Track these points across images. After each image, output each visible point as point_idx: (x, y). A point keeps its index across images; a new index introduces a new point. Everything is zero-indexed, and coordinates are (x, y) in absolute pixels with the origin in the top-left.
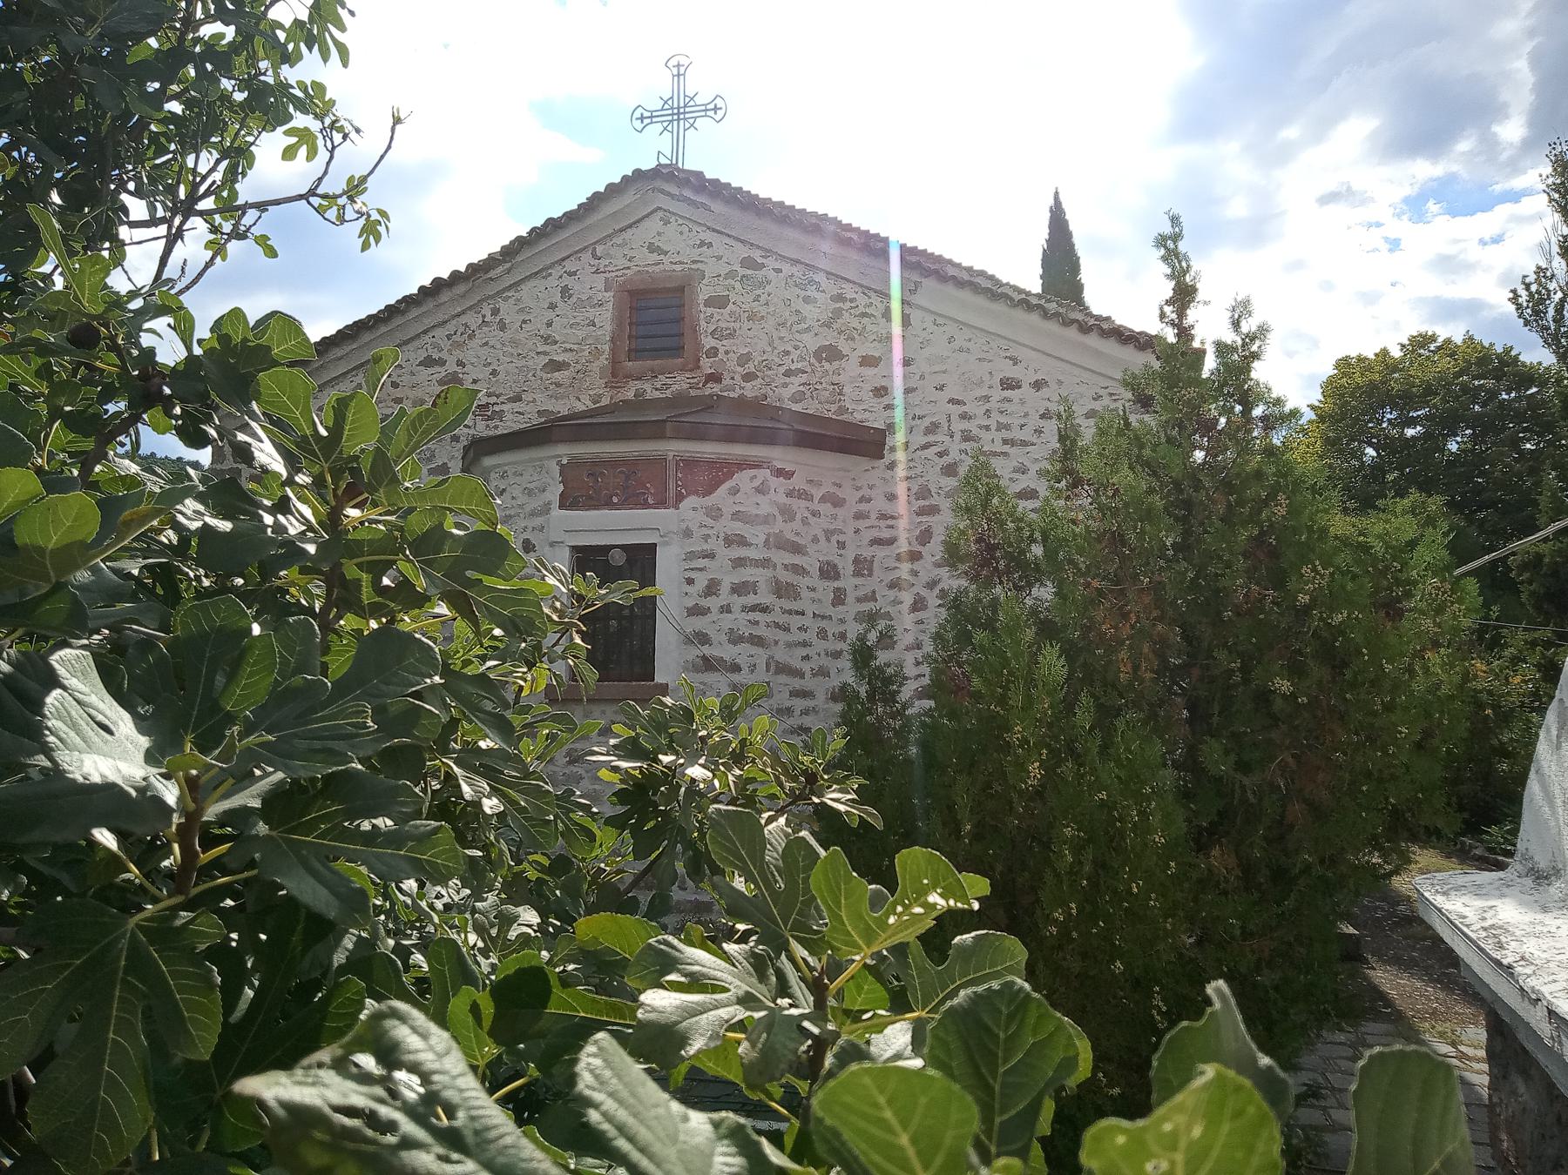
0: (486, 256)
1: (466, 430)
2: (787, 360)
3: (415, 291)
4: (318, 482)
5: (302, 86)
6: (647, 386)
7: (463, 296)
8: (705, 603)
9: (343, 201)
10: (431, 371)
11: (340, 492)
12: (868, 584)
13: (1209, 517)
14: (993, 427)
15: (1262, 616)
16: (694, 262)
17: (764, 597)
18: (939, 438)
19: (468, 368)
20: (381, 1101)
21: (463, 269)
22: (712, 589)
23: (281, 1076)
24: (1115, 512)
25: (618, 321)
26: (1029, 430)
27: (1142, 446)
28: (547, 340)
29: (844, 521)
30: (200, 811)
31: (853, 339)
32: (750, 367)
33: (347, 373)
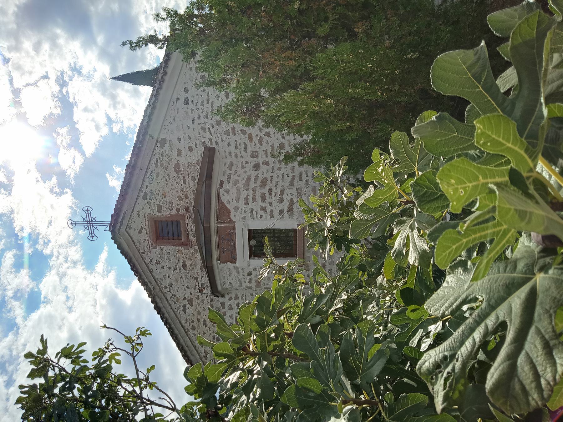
0: (145, 291)
1: (209, 296)
2: (180, 183)
3: (159, 315)
4: (242, 360)
5: (94, 359)
6: (191, 233)
7: (160, 299)
8: (269, 212)
9: (134, 344)
10: (187, 309)
11: (245, 353)
12: (261, 153)
13: (236, 31)
14: (202, 107)
15: (272, 12)
16: (145, 217)
17: (266, 191)
18: (207, 127)
19: (186, 296)
20: (442, 375)
21: (150, 299)
22: (264, 209)
23: (436, 401)
24: (235, 67)
25: (166, 244)
26: (203, 94)
27: (210, 56)
28: (175, 269)
29: (238, 162)
30: (353, 400)
31: (171, 159)
32: (183, 196)
33: (189, 338)
